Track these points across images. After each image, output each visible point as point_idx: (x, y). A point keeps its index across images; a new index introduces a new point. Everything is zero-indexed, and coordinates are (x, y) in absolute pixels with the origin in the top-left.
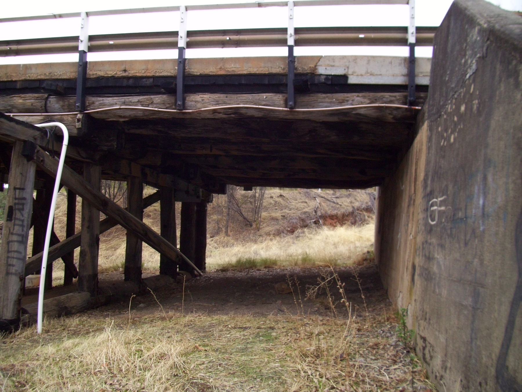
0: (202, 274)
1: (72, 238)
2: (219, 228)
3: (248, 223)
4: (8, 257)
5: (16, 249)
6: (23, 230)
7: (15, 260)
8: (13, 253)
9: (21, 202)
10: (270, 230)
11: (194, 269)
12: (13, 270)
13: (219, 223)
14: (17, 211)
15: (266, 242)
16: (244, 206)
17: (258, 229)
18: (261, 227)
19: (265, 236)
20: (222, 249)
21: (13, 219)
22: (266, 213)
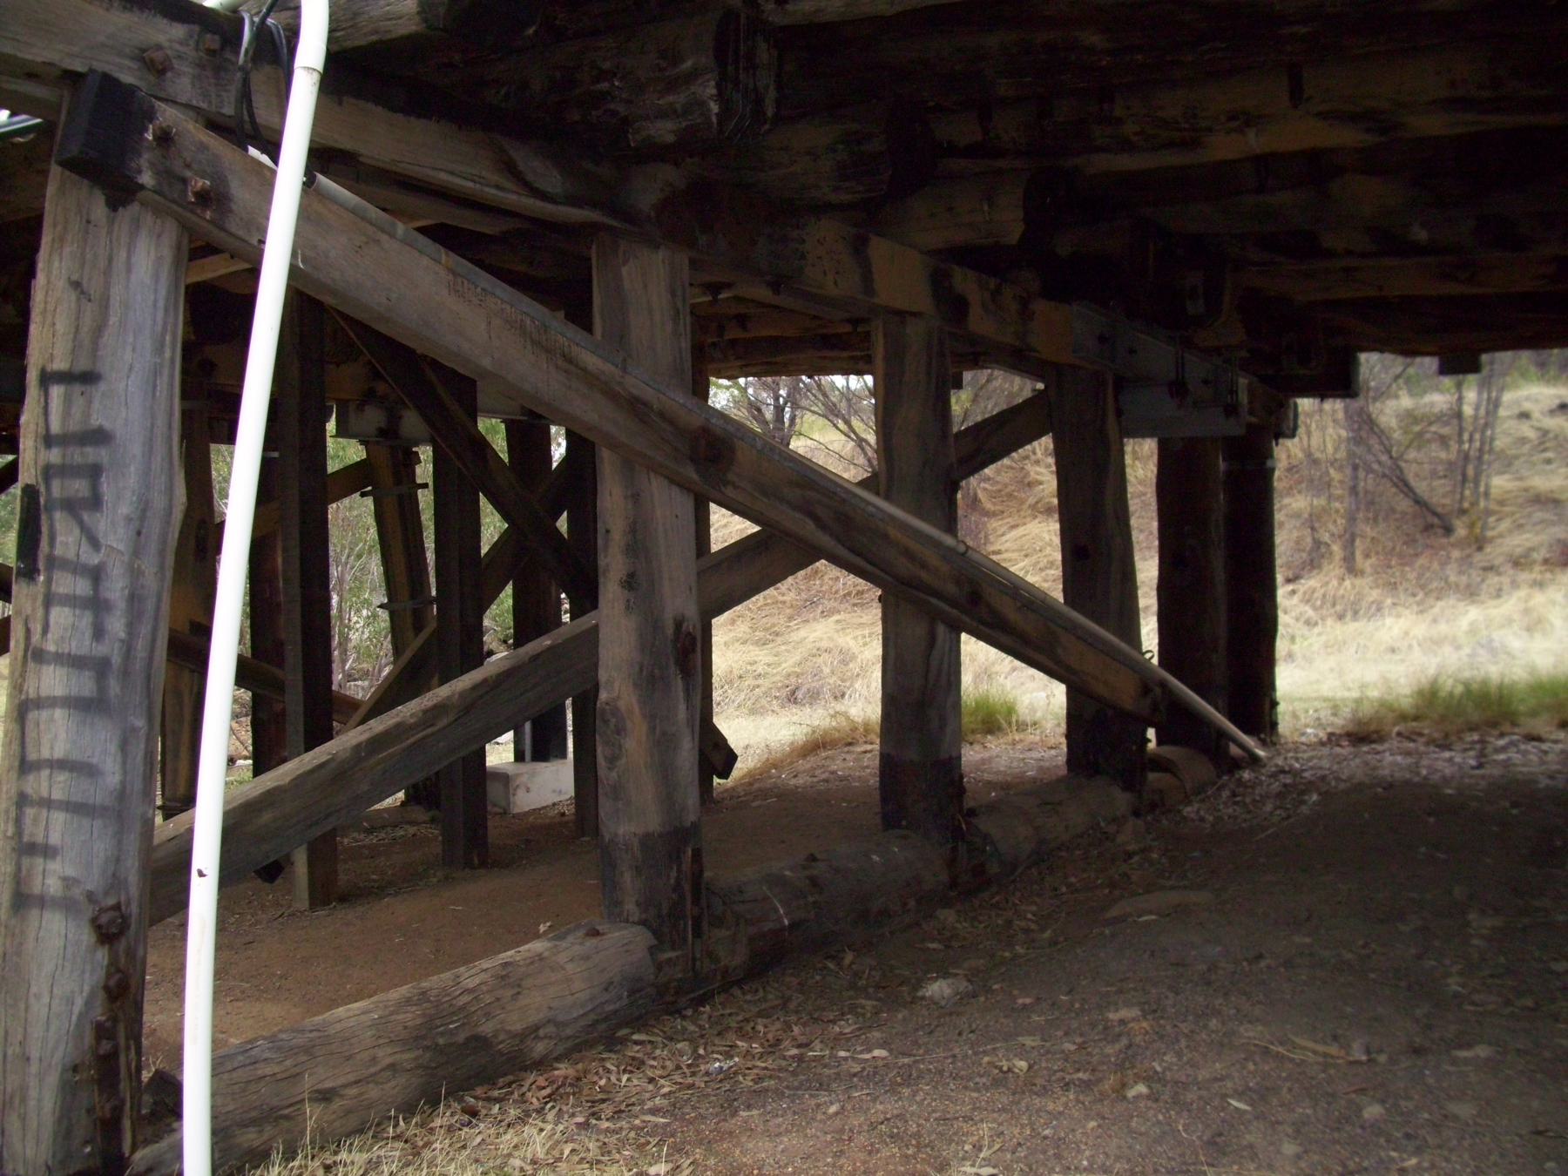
0: (1261, 753)
1: (549, 642)
2: (1318, 544)
3: (1436, 521)
4: (22, 800)
5: (59, 752)
6: (99, 633)
7: (59, 818)
8: (45, 773)
9: (78, 456)
10: (1528, 544)
11: (1223, 735)
12: (50, 877)
13: (1317, 525)
14: (58, 515)
15: (1522, 593)
16: (1412, 454)
17: (1480, 543)
18: (1489, 534)
19: (1511, 572)
20: (1336, 630)
21: (41, 565)
22: (1507, 476)
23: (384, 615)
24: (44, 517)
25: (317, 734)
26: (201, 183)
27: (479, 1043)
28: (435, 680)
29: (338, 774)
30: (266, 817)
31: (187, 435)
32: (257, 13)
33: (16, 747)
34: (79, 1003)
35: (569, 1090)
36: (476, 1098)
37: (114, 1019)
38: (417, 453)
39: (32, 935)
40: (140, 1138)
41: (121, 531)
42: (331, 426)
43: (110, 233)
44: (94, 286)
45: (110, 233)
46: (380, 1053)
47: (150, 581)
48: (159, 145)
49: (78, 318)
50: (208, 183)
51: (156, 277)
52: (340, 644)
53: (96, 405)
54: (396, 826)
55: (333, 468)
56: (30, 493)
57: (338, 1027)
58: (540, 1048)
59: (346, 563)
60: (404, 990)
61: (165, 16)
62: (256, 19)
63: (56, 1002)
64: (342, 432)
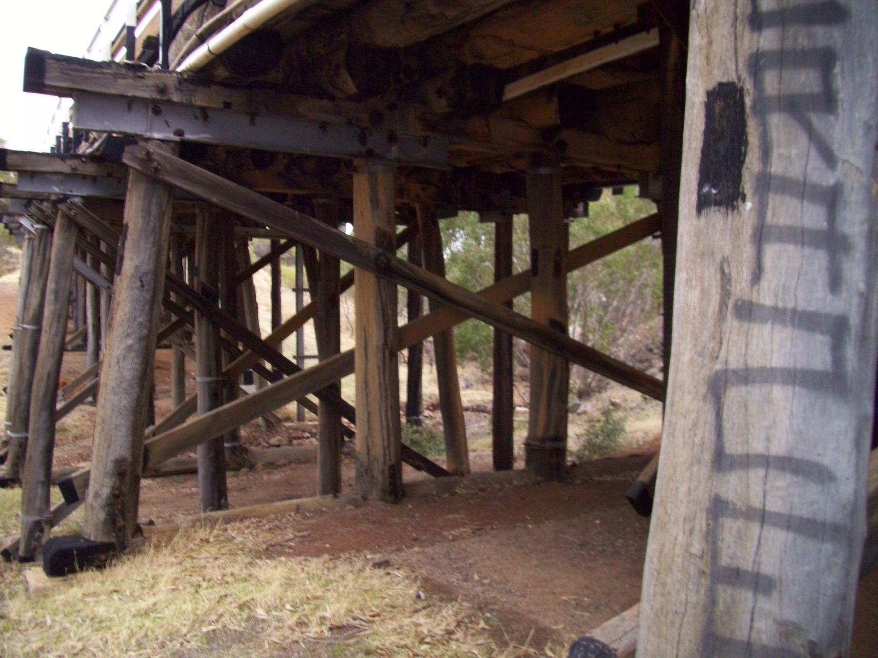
6: (835, 282)
14: (776, 121)
21: (748, 185)
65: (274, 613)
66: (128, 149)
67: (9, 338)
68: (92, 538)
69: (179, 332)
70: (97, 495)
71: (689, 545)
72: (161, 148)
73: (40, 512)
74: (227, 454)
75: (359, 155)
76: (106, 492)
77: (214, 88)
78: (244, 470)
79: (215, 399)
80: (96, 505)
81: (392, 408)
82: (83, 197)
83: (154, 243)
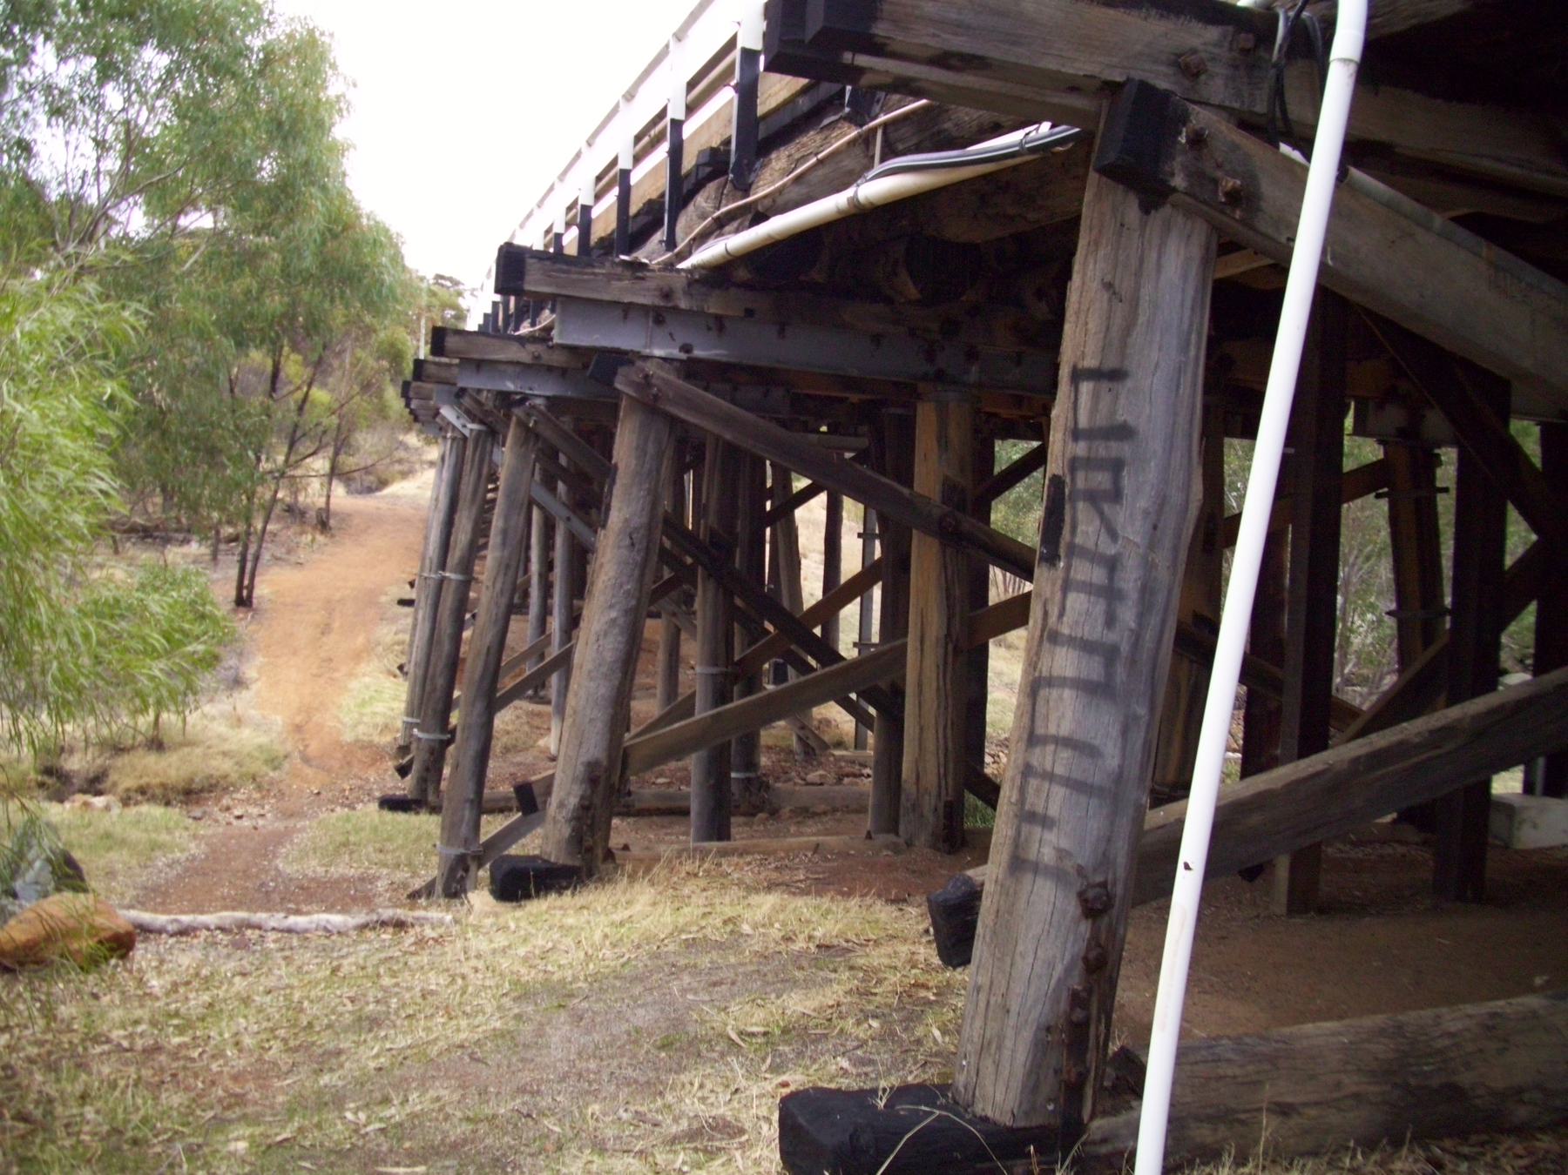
5: (1065, 729)
6: (1110, 620)
7: (1059, 792)
8: (1050, 748)
9: (1103, 450)
14: (1081, 505)
21: (1062, 552)
23: (1391, 622)
24: (1067, 507)
25: (1312, 742)
26: (1230, 183)
27: (1454, 1092)
28: (1442, 698)
29: (1335, 784)
30: (1255, 819)
31: (1205, 433)
32: (1291, 8)
33: (1026, 720)
34: (1059, 969)
35: (1550, 1166)
36: (1443, 1150)
37: (1090, 991)
38: (1438, 456)
39: (1024, 898)
40: (1099, 1108)
41: (1138, 524)
42: (1349, 422)
43: (1142, 235)
44: (1125, 286)
45: (1142, 235)
46: (1346, 1079)
47: (1163, 574)
48: (1191, 147)
49: (1109, 318)
50: (1238, 182)
51: (1185, 277)
52: (1341, 646)
53: (1122, 401)
54: (1384, 843)
55: (1348, 465)
56: (1057, 482)
57: (1305, 1043)
58: (1522, 1113)
59: (1353, 565)
60: (1379, 1020)
61: (1200, 21)
62: (1292, 14)
63: (1039, 963)
64: (1360, 430)
65: (761, 930)
66: (622, 370)
67: (408, 587)
68: (553, 859)
69: (674, 594)
70: (561, 805)
71: (1010, 797)
72: (662, 368)
73: (466, 842)
74: (734, 788)
75: (925, 378)
76: (573, 801)
77: (733, 291)
78: (761, 815)
79: (721, 696)
80: (559, 817)
81: (952, 724)
82: (548, 398)
83: (649, 490)
